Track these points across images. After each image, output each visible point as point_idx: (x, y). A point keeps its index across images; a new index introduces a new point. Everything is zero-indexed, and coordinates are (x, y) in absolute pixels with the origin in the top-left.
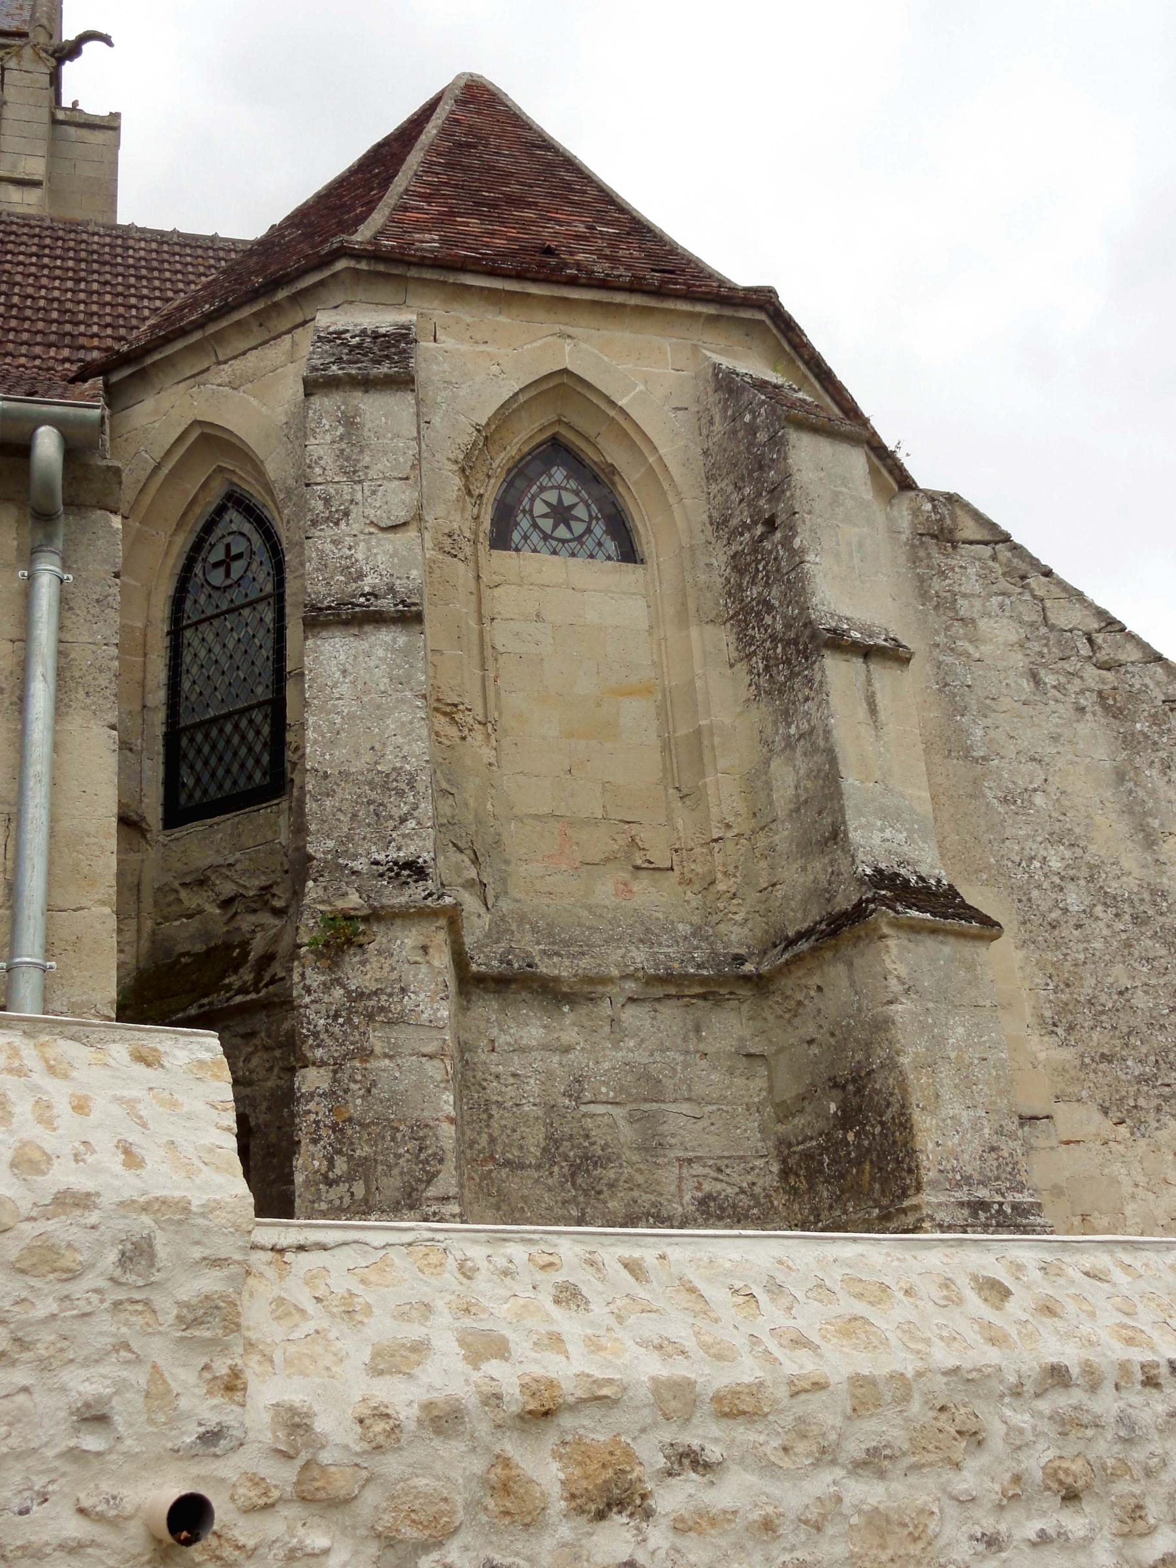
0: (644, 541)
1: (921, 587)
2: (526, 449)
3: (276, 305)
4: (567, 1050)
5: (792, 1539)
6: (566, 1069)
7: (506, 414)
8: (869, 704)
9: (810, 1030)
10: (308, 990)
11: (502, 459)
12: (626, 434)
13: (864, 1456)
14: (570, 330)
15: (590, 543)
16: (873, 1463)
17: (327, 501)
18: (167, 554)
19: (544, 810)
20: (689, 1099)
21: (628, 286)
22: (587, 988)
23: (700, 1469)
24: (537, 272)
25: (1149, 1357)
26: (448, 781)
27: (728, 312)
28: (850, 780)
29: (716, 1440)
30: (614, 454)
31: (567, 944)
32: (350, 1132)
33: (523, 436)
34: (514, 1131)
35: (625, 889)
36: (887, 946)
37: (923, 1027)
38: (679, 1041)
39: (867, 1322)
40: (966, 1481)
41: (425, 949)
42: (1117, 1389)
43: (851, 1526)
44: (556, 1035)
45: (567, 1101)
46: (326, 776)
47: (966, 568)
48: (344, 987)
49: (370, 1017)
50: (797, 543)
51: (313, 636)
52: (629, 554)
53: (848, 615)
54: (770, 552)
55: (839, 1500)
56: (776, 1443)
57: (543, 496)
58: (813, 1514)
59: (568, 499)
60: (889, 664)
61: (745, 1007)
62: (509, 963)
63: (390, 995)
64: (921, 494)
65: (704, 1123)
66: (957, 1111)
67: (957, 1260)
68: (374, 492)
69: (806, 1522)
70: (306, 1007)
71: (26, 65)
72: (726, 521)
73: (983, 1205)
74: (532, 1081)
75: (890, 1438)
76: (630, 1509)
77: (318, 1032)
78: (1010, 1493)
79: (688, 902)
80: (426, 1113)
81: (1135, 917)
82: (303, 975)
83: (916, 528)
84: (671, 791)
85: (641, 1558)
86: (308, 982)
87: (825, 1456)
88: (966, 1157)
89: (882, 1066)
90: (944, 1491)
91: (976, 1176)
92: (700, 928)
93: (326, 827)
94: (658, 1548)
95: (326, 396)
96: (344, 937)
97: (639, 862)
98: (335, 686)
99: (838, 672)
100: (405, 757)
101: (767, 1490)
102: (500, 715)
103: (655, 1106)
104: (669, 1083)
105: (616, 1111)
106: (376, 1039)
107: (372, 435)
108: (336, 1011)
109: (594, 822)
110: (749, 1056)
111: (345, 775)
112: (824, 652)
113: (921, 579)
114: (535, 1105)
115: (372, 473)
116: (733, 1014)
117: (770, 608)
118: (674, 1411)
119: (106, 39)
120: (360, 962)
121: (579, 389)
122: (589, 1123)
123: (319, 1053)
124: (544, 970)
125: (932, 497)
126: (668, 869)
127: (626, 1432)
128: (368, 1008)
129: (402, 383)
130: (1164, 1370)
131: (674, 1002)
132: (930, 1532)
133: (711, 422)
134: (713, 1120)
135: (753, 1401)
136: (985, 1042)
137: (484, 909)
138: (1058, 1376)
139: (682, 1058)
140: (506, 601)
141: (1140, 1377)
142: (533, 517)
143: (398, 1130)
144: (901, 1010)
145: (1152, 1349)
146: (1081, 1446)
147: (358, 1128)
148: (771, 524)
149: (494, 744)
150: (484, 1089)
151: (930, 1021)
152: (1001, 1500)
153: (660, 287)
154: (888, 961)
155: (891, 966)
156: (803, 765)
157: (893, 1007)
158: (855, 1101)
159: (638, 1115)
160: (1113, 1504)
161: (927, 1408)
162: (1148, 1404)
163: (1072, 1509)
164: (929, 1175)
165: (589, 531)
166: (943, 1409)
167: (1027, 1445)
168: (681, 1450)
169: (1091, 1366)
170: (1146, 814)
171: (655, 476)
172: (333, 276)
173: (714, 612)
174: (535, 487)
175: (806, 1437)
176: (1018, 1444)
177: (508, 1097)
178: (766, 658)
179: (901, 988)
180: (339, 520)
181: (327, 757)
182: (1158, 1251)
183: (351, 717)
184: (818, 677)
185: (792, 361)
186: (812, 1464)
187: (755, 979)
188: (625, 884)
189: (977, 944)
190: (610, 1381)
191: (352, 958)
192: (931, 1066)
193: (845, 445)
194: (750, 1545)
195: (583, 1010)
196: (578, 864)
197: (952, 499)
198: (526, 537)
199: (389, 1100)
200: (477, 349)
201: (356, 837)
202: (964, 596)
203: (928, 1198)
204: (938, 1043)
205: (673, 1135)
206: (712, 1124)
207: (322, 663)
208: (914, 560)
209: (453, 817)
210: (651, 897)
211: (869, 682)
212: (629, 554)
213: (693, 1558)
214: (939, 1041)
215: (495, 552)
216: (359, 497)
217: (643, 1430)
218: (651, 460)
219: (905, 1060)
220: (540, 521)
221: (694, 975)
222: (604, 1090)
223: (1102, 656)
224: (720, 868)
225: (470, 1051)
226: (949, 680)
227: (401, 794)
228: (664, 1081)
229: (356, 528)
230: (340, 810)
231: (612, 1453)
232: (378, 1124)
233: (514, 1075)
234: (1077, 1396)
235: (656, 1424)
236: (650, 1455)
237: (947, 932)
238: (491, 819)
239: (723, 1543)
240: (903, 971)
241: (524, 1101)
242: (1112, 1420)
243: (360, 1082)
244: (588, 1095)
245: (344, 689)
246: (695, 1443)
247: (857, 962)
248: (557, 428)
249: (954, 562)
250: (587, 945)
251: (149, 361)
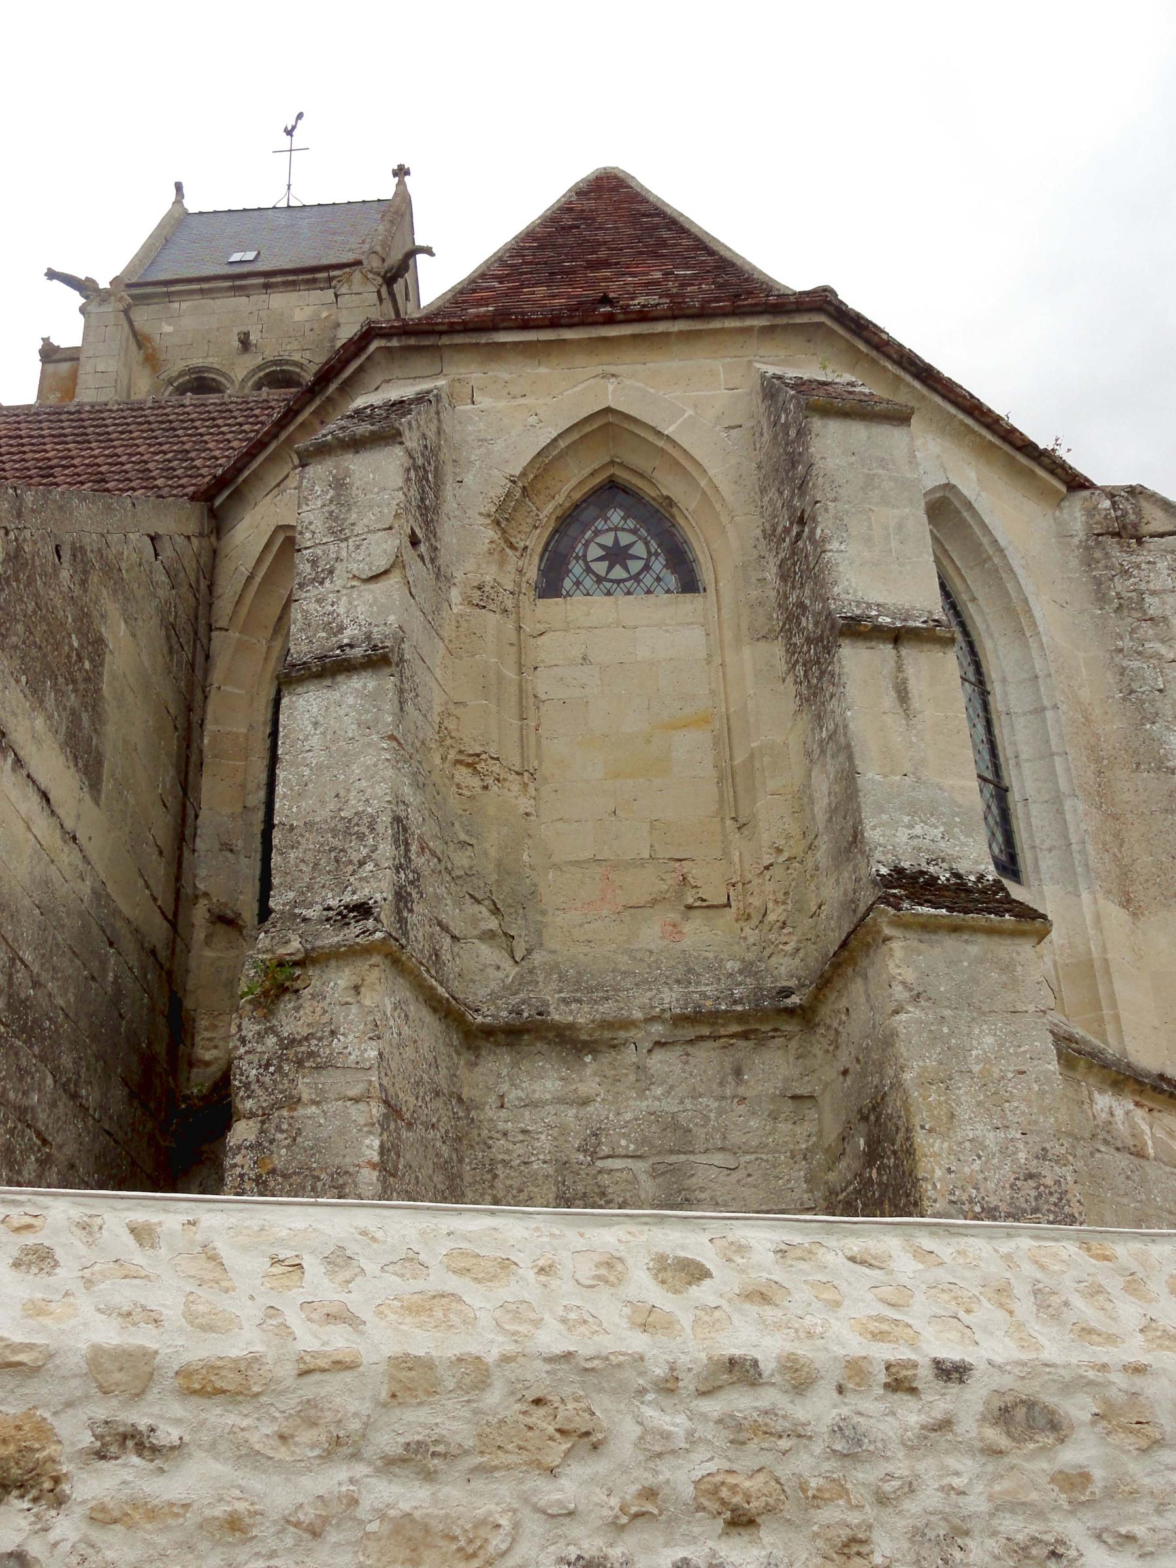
0: (704, 569)
1: (1098, 591)
2: (577, 496)
3: (329, 399)
4: (585, 1102)
5: (272, 1543)
6: (584, 1123)
7: (546, 463)
8: (899, 692)
10: (243, 1041)
11: (548, 510)
12: (677, 463)
13: (400, 1451)
14: (613, 369)
15: (648, 580)
16: (418, 1459)
17: (314, 563)
18: (266, 659)
19: (587, 855)
20: (722, 1149)
21: (670, 313)
22: (607, 1035)
23: (146, 1453)
24: (570, 317)
25: (904, 1353)
26: (467, 832)
28: (870, 775)
29: (178, 1422)
30: (670, 486)
31: (590, 990)
32: (272, 1184)
33: (572, 482)
34: (521, 1191)
36: (891, 949)
37: (935, 1038)
38: (715, 1086)
39: (456, 1298)
40: (567, 1489)
41: (356, 989)
42: (840, 1392)
43: (367, 1534)
44: (574, 1087)
45: (581, 1157)
46: (292, 828)
47: (1155, 563)
48: (276, 1034)
49: (300, 1063)
51: (290, 693)
52: (690, 584)
53: (881, 601)
54: (802, 550)
55: (354, 1502)
56: (268, 1429)
57: (598, 540)
58: (308, 1515)
59: (625, 539)
60: (926, 647)
61: (794, 1044)
62: (519, 1013)
63: (320, 1039)
64: (1097, 492)
65: (741, 1173)
66: (979, 1133)
67: (644, 1238)
68: (358, 547)
69: (297, 1525)
70: (241, 1058)
71: (356, 288)
74: (543, 1137)
75: (444, 1432)
76: (34, 1493)
77: (250, 1083)
78: (634, 1510)
79: (745, 938)
80: (347, 1160)
82: (240, 1027)
83: (1091, 528)
84: (728, 822)
85: (35, 1549)
86: (244, 1033)
87: (340, 1447)
88: (991, 1185)
89: (892, 1086)
90: (526, 1501)
91: (1003, 1207)
92: (752, 964)
93: (289, 879)
94: (63, 1540)
95: (320, 463)
96: (281, 983)
97: (690, 901)
98: (306, 739)
99: (854, 660)
100: (367, 800)
101: (243, 1483)
102: (540, 764)
103: (682, 1158)
104: (701, 1133)
105: (640, 1166)
106: (304, 1087)
107: (359, 492)
108: (268, 1060)
110: (794, 1097)
111: (309, 825)
112: (841, 641)
113: (1098, 582)
114: (545, 1162)
115: (358, 529)
116: (780, 1052)
118: (117, 1385)
120: (294, 1008)
121: (626, 426)
122: (605, 1179)
123: (249, 1104)
124: (557, 1017)
125: (1111, 494)
126: (725, 906)
127: (46, 1405)
128: (300, 1054)
129: (389, 437)
130: (925, 1372)
131: (710, 1044)
132: (491, 1549)
133: (762, 434)
134: (750, 1171)
135: (239, 1378)
136: (1025, 1052)
137: (511, 962)
138: (740, 1371)
139: (716, 1104)
140: (548, 649)
141: (883, 1378)
142: (586, 563)
143: (318, 1179)
145: (912, 1346)
146: (766, 1459)
147: (280, 1180)
149: (534, 793)
150: (490, 1147)
151: (945, 1030)
152: (617, 1517)
153: (702, 307)
154: (891, 965)
155: (894, 971)
157: (897, 1017)
159: (662, 1168)
160: (816, 1535)
161: (512, 1399)
162: (894, 1414)
163: (746, 1538)
165: (647, 568)
166: (538, 1402)
167: (673, 1452)
168: (121, 1429)
169: (796, 1361)
172: (368, 358)
173: (767, 628)
174: (589, 532)
175: (316, 1424)
176: (656, 1448)
177: (515, 1155)
179: (907, 995)
180: (324, 579)
181: (294, 810)
182: (991, 1238)
183: (320, 766)
185: (874, 362)
186: (320, 1456)
187: (799, 1011)
188: (674, 926)
189: (1017, 941)
190: (30, 1347)
191: (287, 1004)
192: (946, 1082)
193: (887, 427)
194: (204, 1546)
195: (606, 1058)
196: (620, 908)
197: (1135, 492)
198: (578, 583)
199: (312, 1149)
200: (515, 403)
201: (316, 886)
202: (1153, 593)
204: (956, 1055)
205: (702, 1189)
206: (749, 1175)
207: (296, 719)
208: (1089, 562)
209: (471, 868)
210: (702, 937)
211: (899, 668)
212: (690, 584)
213: (110, 1555)
215: (540, 602)
216: (344, 554)
217: (69, 1404)
218: (703, 484)
220: (594, 566)
221: (726, 1012)
222: (623, 1142)
224: (771, 897)
225: (478, 1108)
226: (1134, 686)
227: (361, 837)
228: (694, 1130)
229: (339, 583)
230: (303, 861)
231: (19, 1428)
232: (299, 1174)
233: (524, 1132)
234: (768, 1397)
235: (88, 1397)
236: (74, 1432)
237: (974, 930)
238: (527, 870)
239: (162, 1540)
240: (910, 975)
241: (533, 1159)
242: (825, 1429)
243: (286, 1131)
244: (606, 1150)
245: (315, 741)
246: (143, 1423)
247: (870, 973)
248: (612, 471)
249: (1139, 559)
250: (614, 990)
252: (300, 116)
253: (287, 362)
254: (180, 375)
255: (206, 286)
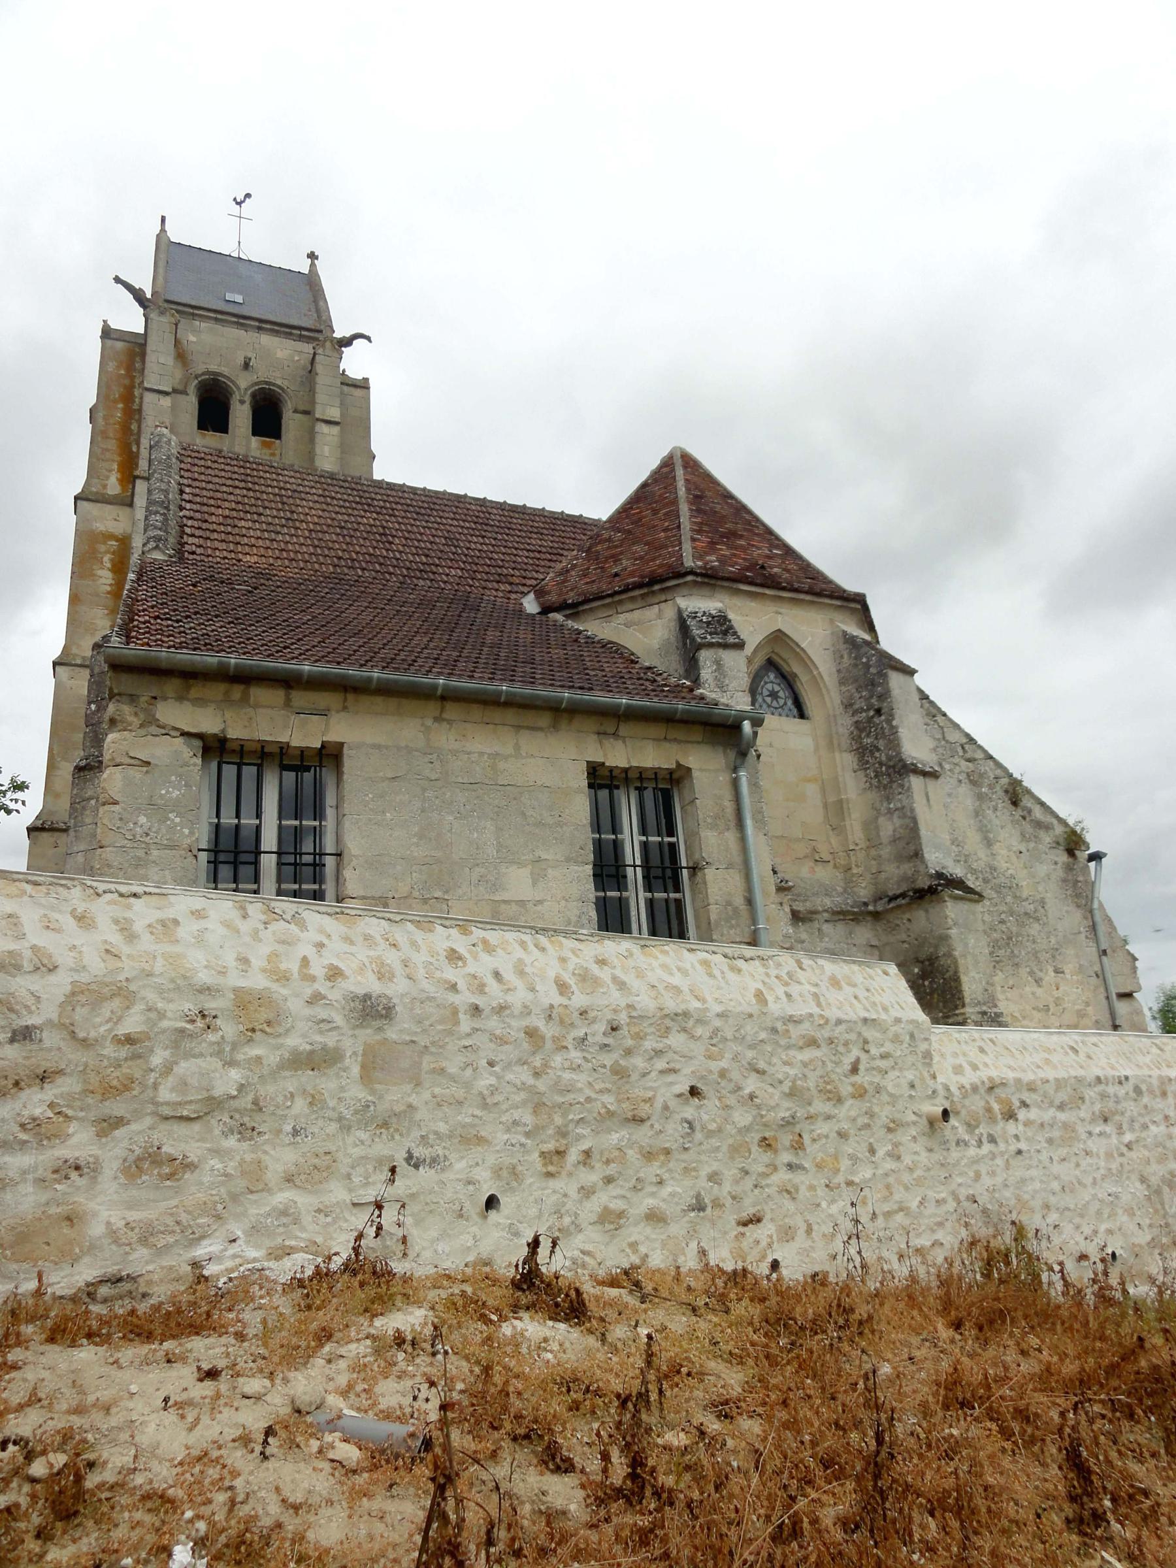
9: (904, 937)
14: (781, 610)
16: (1061, 1107)
27: (845, 604)
30: (796, 668)
35: (813, 871)
50: (894, 723)
59: (777, 688)
71: (328, 352)
72: (851, 705)
73: (984, 1013)
81: (984, 879)
99: (916, 782)
109: (798, 840)
117: (878, 750)
119: (368, 339)
144: (953, 932)
148: (878, 712)
156: (897, 822)
158: (929, 969)
164: (967, 1000)
165: (785, 704)
170: (988, 831)
171: (816, 681)
178: (876, 771)
184: (907, 785)
192: (964, 956)
195: (808, 925)
203: (969, 1010)
212: (802, 715)
214: (966, 945)
219: (956, 953)
223: (968, 756)
247: (931, 910)
251: (581, 608)
252: (248, 196)
253: (274, 385)
254: (203, 374)
255: (219, 316)
